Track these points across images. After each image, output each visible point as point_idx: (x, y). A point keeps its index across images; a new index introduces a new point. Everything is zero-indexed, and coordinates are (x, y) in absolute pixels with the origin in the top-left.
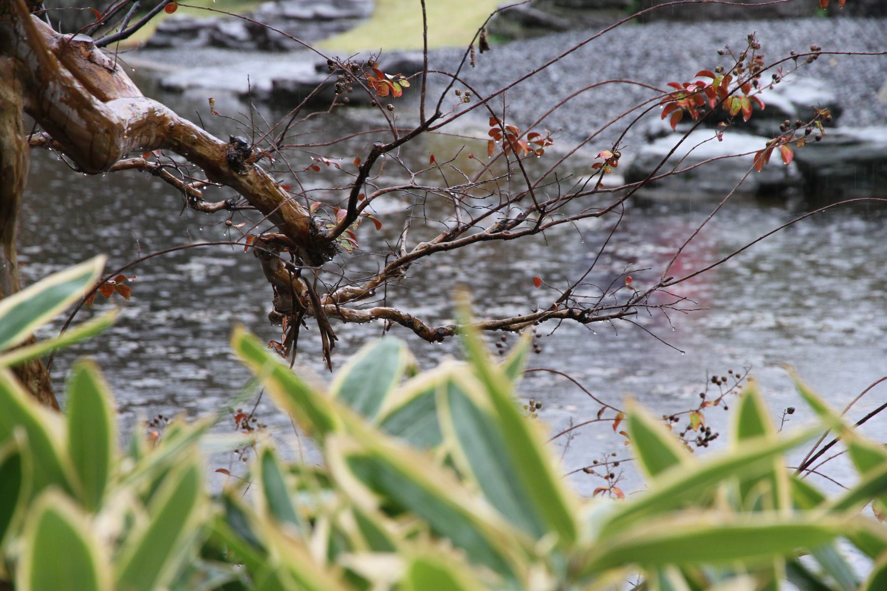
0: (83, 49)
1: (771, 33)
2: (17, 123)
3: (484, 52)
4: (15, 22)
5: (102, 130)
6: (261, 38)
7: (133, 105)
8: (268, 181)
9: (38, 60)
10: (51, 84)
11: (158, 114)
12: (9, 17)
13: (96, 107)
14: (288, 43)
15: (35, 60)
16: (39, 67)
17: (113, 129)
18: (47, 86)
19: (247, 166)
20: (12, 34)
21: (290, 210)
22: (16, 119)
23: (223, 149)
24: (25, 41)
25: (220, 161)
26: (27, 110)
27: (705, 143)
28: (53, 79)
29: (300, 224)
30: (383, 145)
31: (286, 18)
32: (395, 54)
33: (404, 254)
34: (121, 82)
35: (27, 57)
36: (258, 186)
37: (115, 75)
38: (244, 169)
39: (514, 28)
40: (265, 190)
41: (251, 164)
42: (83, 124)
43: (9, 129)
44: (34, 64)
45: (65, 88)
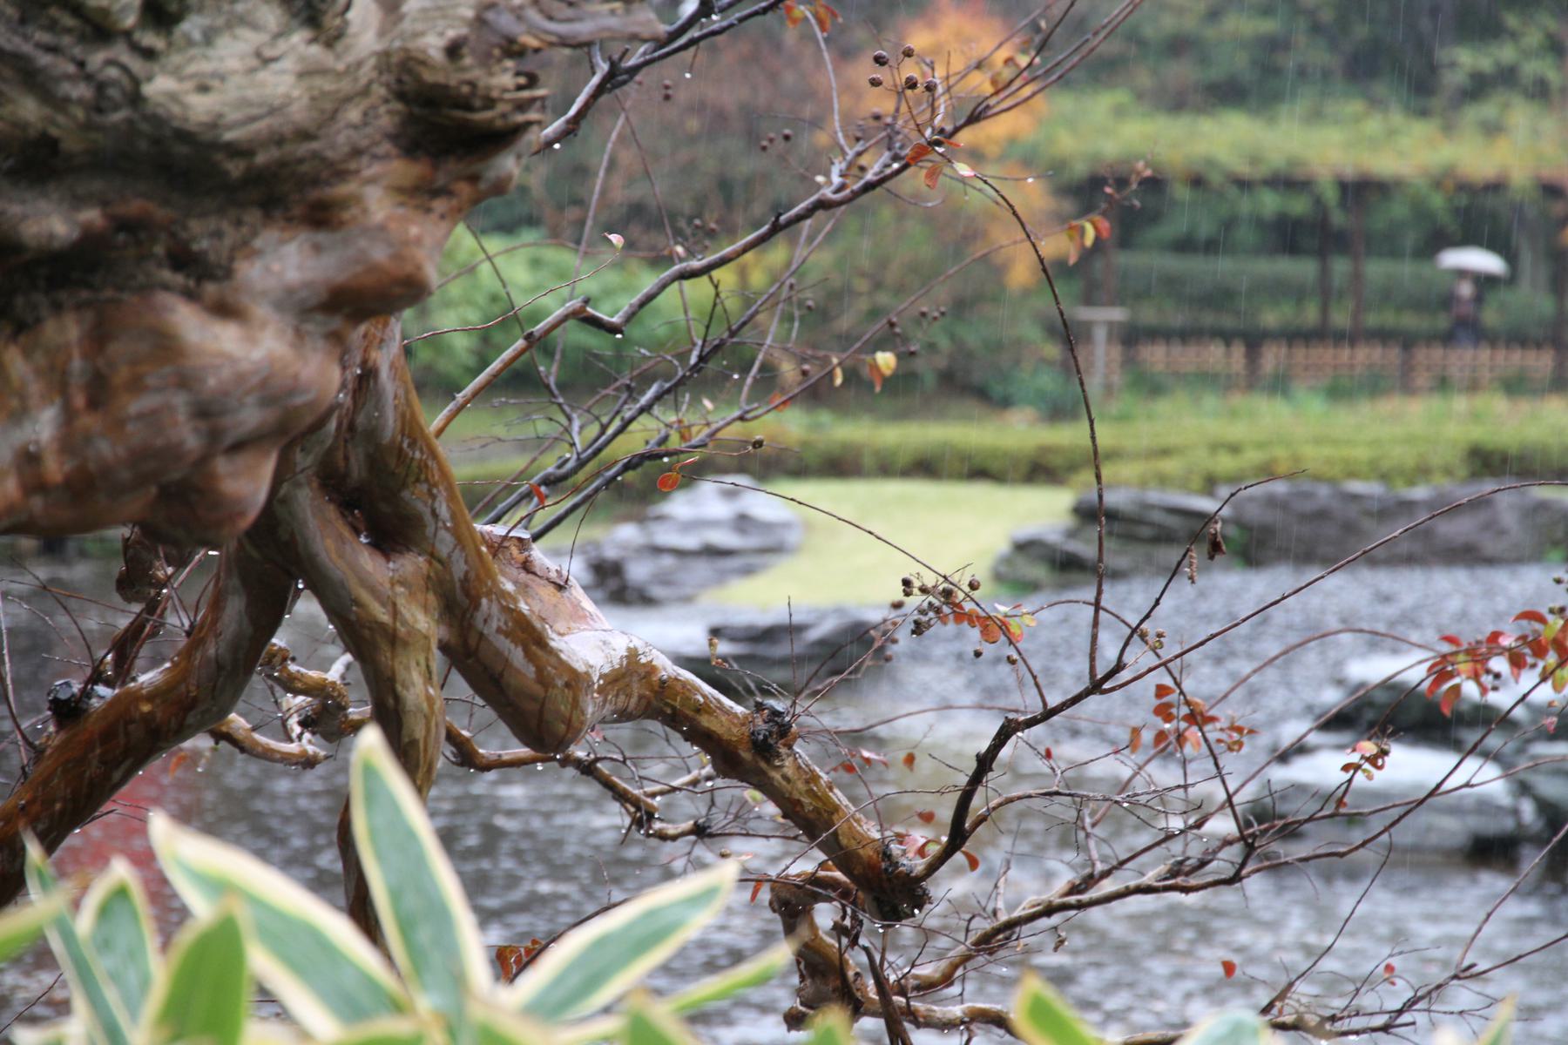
0: (515, 551)
1: (1475, 589)
2: (428, 666)
3: (1217, 557)
4: (434, 497)
5: (560, 683)
6: (613, 584)
7: (604, 643)
8: (815, 778)
9: (466, 562)
10: (484, 601)
11: (644, 660)
12: (424, 487)
13: (552, 644)
14: (657, 591)
15: (462, 562)
16: (467, 573)
17: (576, 681)
18: (477, 606)
19: (783, 750)
20: (428, 517)
21: (851, 827)
22: (427, 659)
23: (745, 722)
24: (447, 529)
25: (740, 741)
26: (444, 647)
27: (1411, 766)
28: (489, 594)
29: (866, 853)
30: (1022, 718)
31: (657, 550)
32: (839, 611)
33: (1003, 917)
34: (577, 606)
35: (449, 556)
36: (801, 786)
37: (566, 594)
38: (778, 755)
39: (1039, 572)
40: (810, 792)
41: (790, 747)
42: (530, 671)
43: (416, 677)
44: (459, 568)
45: (506, 610)
